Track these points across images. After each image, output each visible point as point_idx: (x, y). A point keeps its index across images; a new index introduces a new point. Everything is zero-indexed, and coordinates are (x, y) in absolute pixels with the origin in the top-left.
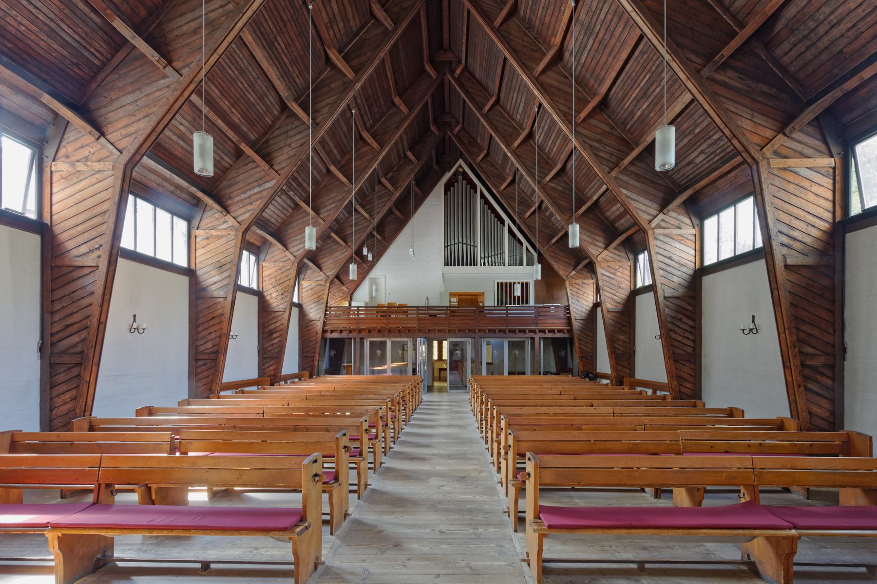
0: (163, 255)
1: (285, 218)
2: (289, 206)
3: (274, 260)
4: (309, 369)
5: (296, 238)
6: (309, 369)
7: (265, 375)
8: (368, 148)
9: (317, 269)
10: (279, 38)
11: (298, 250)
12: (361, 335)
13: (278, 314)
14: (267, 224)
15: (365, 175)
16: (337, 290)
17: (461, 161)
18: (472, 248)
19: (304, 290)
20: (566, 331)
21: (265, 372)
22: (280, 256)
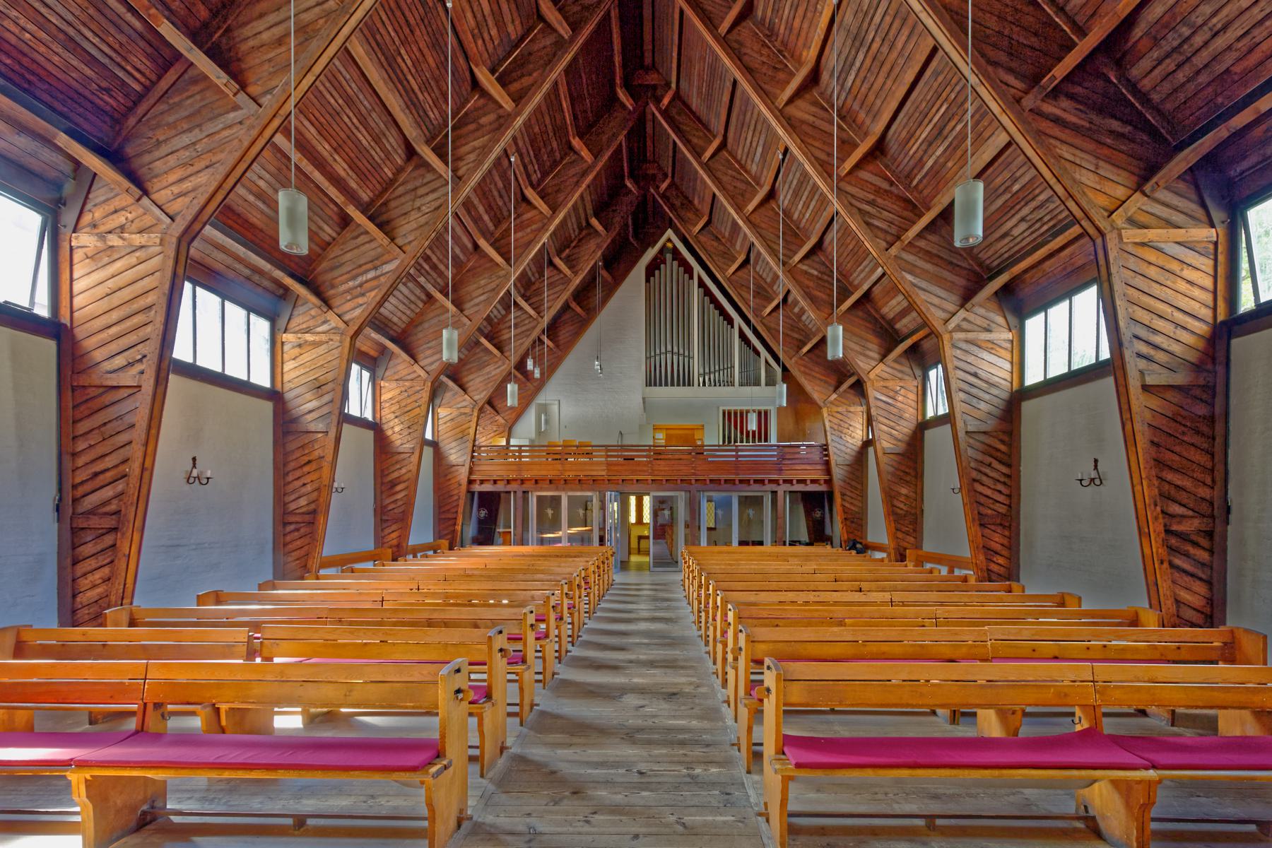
0: (236, 370)
1: (412, 315)
3: (396, 377)
4: (449, 536)
6: (449, 536)
8: (534, 212)
10: (403, 51)
12: (525, 487)
13: (403, 456)
14: (386, 325)
17: (670, 233)
18: (686, 359)
19: (441, 422)
20: (822, 482)
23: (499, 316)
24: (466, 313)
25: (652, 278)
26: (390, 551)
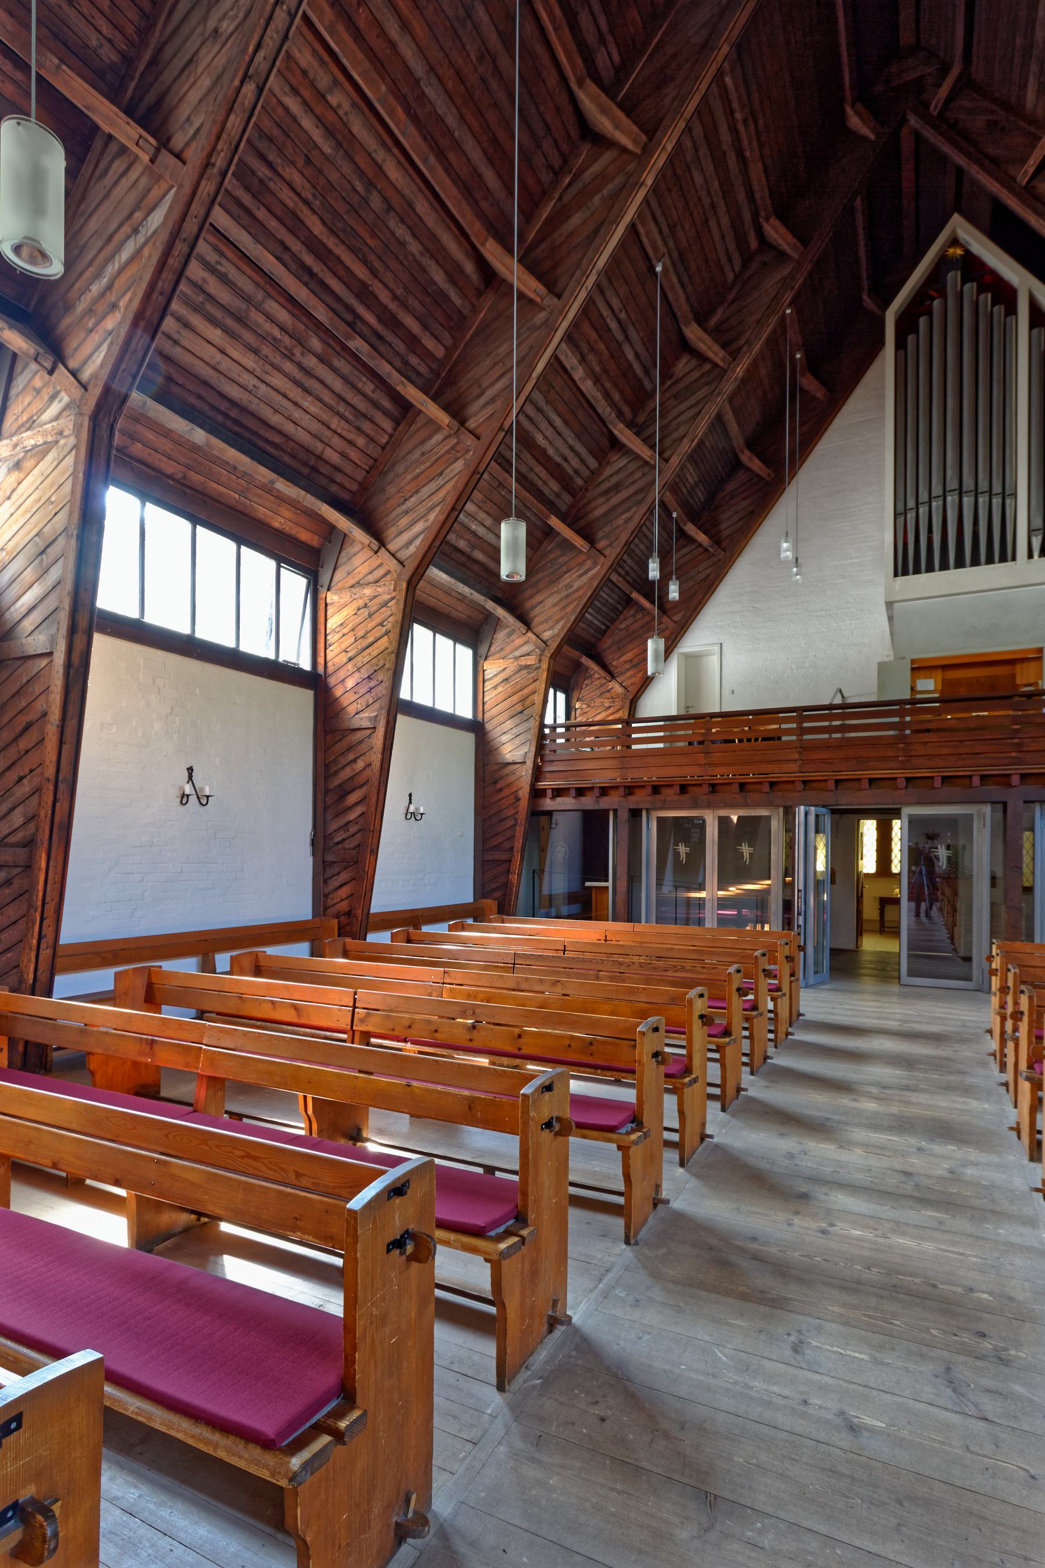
0: (444, 705)
1: (374, 451)
2: (375, 405)
3: (351, 582)
4: (498, 894)
5: (404, 507)
6: (498, 894)
7: (329, 911)
8: (608, 156)
9: (519, 624)
11: (410, 543)
12: (633, 802)
13: (359, 735)
14: (314, 469)
15: (599, 252)
16: (598, 693)
17: (959, 226)
18: (996, 501)
19: (488, 685)
21: (330, 902)
22: (363, 570)
23: (586, 473)
24: (472, 424)
25: (911, 338)
26: (335, 922)
